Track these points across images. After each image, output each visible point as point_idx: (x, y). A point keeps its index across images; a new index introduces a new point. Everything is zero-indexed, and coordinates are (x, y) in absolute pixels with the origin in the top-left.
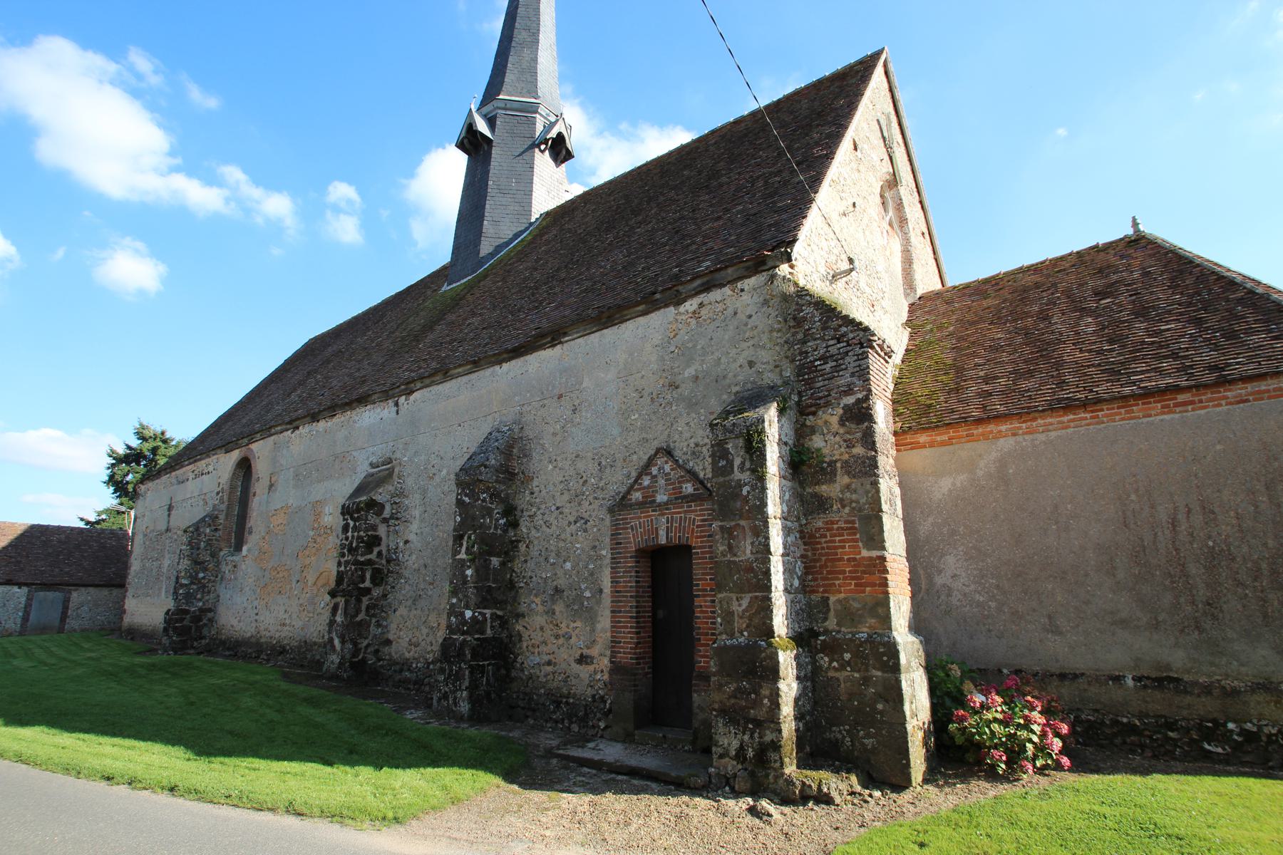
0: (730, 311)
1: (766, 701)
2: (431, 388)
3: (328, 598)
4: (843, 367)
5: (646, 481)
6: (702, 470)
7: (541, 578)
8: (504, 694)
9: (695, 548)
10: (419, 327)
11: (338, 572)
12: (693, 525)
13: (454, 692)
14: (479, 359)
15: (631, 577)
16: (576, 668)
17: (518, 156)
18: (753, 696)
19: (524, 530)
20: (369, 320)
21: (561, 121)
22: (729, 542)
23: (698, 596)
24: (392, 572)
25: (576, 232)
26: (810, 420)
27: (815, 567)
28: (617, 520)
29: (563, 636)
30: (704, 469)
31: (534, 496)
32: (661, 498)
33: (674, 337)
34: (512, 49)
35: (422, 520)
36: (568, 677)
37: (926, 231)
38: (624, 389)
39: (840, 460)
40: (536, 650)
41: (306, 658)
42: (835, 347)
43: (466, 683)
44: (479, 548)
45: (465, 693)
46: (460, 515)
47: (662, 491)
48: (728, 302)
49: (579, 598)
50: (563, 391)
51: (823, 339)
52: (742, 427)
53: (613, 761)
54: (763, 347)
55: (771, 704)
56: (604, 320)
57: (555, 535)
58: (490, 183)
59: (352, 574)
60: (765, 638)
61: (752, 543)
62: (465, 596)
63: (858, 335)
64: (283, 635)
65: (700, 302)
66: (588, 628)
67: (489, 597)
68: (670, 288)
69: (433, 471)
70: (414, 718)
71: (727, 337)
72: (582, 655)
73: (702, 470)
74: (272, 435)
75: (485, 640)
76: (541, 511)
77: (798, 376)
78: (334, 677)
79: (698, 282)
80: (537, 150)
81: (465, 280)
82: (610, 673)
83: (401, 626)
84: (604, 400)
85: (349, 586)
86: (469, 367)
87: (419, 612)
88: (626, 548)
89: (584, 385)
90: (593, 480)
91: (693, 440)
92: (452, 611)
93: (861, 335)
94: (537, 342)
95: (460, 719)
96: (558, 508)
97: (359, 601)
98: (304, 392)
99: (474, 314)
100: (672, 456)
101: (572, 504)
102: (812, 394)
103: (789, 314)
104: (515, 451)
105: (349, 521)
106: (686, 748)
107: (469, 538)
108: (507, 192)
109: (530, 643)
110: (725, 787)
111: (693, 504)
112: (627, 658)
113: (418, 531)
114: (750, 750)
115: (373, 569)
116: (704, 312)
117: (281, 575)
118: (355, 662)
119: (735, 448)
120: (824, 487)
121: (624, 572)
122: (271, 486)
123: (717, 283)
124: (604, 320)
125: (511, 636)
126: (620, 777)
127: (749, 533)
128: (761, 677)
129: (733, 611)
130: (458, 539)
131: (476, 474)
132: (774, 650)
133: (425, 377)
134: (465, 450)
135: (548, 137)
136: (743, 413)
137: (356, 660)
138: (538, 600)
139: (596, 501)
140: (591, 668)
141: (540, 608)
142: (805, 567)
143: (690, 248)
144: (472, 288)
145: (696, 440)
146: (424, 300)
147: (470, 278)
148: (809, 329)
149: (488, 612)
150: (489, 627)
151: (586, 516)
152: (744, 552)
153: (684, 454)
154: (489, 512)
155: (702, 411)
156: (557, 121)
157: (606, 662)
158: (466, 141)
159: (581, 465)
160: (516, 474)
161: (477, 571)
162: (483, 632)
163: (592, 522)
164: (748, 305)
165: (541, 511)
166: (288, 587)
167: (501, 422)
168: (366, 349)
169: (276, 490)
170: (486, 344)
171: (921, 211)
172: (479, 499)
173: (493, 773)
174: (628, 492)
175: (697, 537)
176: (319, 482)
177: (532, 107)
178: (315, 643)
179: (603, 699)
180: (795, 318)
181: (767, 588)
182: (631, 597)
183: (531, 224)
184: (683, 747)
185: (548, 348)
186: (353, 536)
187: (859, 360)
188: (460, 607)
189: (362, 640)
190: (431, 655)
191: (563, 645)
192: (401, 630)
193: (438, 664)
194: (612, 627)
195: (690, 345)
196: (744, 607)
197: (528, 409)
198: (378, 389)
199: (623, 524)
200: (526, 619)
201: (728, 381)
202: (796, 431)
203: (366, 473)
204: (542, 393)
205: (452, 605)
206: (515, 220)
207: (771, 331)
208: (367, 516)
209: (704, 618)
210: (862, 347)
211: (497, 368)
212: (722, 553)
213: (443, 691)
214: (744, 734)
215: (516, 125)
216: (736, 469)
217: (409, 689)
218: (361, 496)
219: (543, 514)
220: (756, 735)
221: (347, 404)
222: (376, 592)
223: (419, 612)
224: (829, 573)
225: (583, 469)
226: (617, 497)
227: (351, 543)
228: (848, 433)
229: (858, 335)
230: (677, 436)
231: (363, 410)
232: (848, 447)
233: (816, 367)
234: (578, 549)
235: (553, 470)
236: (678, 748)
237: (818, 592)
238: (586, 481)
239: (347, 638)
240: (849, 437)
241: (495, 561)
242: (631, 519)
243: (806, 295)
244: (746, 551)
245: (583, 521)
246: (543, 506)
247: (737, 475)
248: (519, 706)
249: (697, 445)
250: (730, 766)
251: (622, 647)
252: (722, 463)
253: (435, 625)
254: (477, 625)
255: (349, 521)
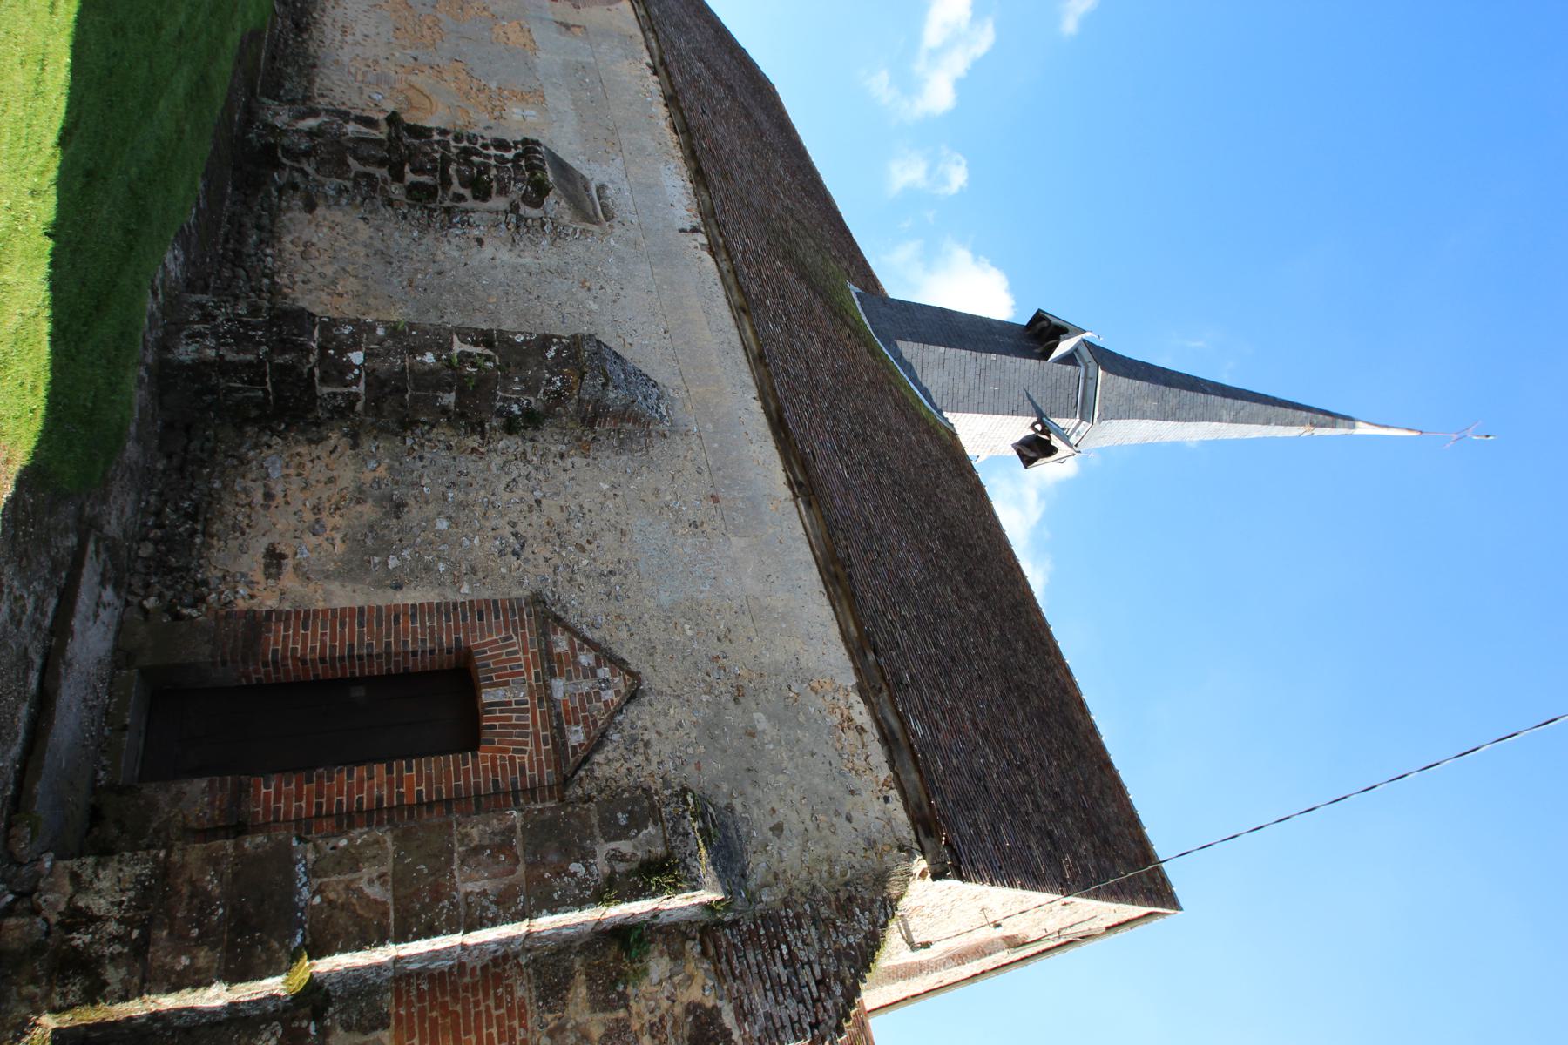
0: (856, 782)
1: (185, 961)
2: (720, 285)
3: (390, 107)
4: (781, 998)
5: (586, 659)
6: (607, 757)
7: (421, 476)
8: (212, 415)
9: (475, 757)
10: (801, 256)
11: (430, 130)
12: (516, 751)
13: (215, 334)
14: (766, 365)
15: (424, 641)
16: (260, 546)
17: (1027, 394)
18: (195, 932)
19: (501, 444)
20: (805, 176)
21: (1069, 451)
22: (485, 847)
23: (390, 771)
24: (430, 216)
25: (938, 487)
26: (692, 948)
27: (443, 993)
28: (521, 610)
29: (317, 521)
30: (609, 761)
31: (557, 460)
32: (559, 687)
33: (813, 689)
34: (1156, 386)
35: (515, 269)
36: (243, 533)
37: (942, 984)
38: (731, 609)
39: (630, 1013)
40: (292, 471)
41: (286, 66)
42: (811, 977)
43: (230, 356)
44: (470, 375)
45: (211, 353)
46: (525, 342)
47: (571, 689)
48: (868, 776)
49: (386, 548)
50: (723, 503)
51: (822, 954)
52: (682, 850)
53: (69, 655)
54: (804, 849)
55: (179, 974)
56: (832, 567)
57: (493, 498)
58: (993, 356)
59: (426, 154)
60: (308, 941)
61: (484, 893)
62: (388, 352)
63: (830, 1017)
64: (328, 30)
65: (865, 727)
66: (331, 566)
67: (387, 390)
68: (884, 678)
69: (595, 288)
70: (165, 266)
71: (817, 780)
72: (283, 556)
73: (607, 757)
74: (643, 32)
75: (310, 385)
76: (533, 473)
77: (763, 917)
78: (250, 116)
79: (895, 724)
80: (1035, 419)
81: (865, 319)
82: (247, 612)
83: (338, 229)
84: (713, 575)
85: (407, 147)
86: (754, 347)
87: (363, 260)
88: (474, 631)
89: (734, 540)
90: (585, 562)
91: (655, 736)
92: (362, 328)
93: (830, 1022)
94: (795, 458)
95: (164, 346)
96: (538, 502)
97: (381, 163)
98: (705, 82)
99: (824, 343)
100: (628, 702)
101: (545, 527)
102: (735, 945)
103: (856, 888)
104: (629, 426)
105: (513, 152)
106: (102, 773)
107: (488, 358)
108: (982, 379)
109: (306, 459)
110: (12, 892)
111: (550, 747)
112: (276, 643)
113: (497, 262)
114: (88, 938)
115: (435, 187)
116: (852, 735)
117: (426, 32)
118: (276, 153)
119: (644, 842)
120: (583, 991)
121: (431, 628)
122: (567, 27)
123: (896, 757)
124: (832, 567)
125: (318, 423)
126: (34, 678)
127: (502, 883)
128: (232, 945)
129: (359, 870)
130: (486, 339)
131: (592, 370)
132: (284, 966)
133: (736, 276)
134: (629, 340)
135: (1052, 435)
136: (705, 845)
137: (280, 155)
138: (382, 472)
139: (551, 570)
140: (258, 576)
141: (368, 476)
142: (442, 973)
143: (935, 691)
144: (857, 336)
145: (654, 742)
146: (835, 257)
147: (869, 326)
148: (836, 928)
149: (361, 388)
150: (334, 390)
151: (527, 553)
152: (469, 879)
153: (632, 722)
154: (531, 389)
155: (702, 749)
156: (1070, 445)
157: (269, 603)
158: (1045, 323)
159: (608, 539)
160: (592, 428)
161: (432, 372)
162: (323, 381)
163: (516, 564)
164: (866, 814)
165: (533, 473)
166: (407, 43)
167: (672, 400)
168: (768, 174)
169: (561, 34)
170: (787, 372)
171: (971, 974)
172: (553, 374)
173: (37, 447)
174: (568, 628)
175: (493, 759)
176: (574, 102)
177: (1089, 413)
178: (311, 82)
179: (200, 600)
180: (850, 899)
181: (402, 937)
182: (388, 644)
183: (940, 412)
184: (104, 768)
185: (787, 476)
186: (488, 157)
187: (793, 1023)
188: (369, 342)
189: (314, 165)
190: (287, 281)
191: (301, 520)
192: (332, 229)
193: (266, 304)
194: (334, 611)
195: (802, 718)
196: (368, 890)
197: (694, 446)
198: (716, 202)
199: (514, 622)
200: (349, 452)
201: (749, 789)
202: (675, 925)
203: (589, 177)
204: (719, 469)
205: (372, 328)
206: (945, 389)
207: (829, 860)
208: (521, 181)
209: (350, 787)
210: (813, 1026)
211: (754, 392)
212: (467, 835)
213: (217, 312)
214: (120, 921)
215: (1066, 392)
216: (613, 845)
217: (227, 241)
218: (554, 172)
219: (528, 477)
220: (117, 948)
221: (693, 152)
222: (396, 190)
223: (363, 260)
224: (434, 1021)
225: (602, 543)
226: (559, 606)
227: (478, 154)
228: (675, 1022)
229: (830, 1017)
230: (660, 708)
231: (685, 177)
232: (652, 1025)
233: (778, 947)
234: (471, 541)
235: (600, 490)
236: (102, 758)
237: (398, 1005)
238: (583, 550)
239: (318, 140)
240: (669, 1025)
241: (449, 399)
242: (524, 636)
243: (886, 915)
244: (471, 883)
245: (517, 547)
246: (541, 476)
247: (603, 849)
248: (190, 441)
249: (647, 744)
250: (54, 900)
251: (296, 633)
252: (622, 818)
253: (340, 289)
254: (338, 369)
255: (513, 152)
